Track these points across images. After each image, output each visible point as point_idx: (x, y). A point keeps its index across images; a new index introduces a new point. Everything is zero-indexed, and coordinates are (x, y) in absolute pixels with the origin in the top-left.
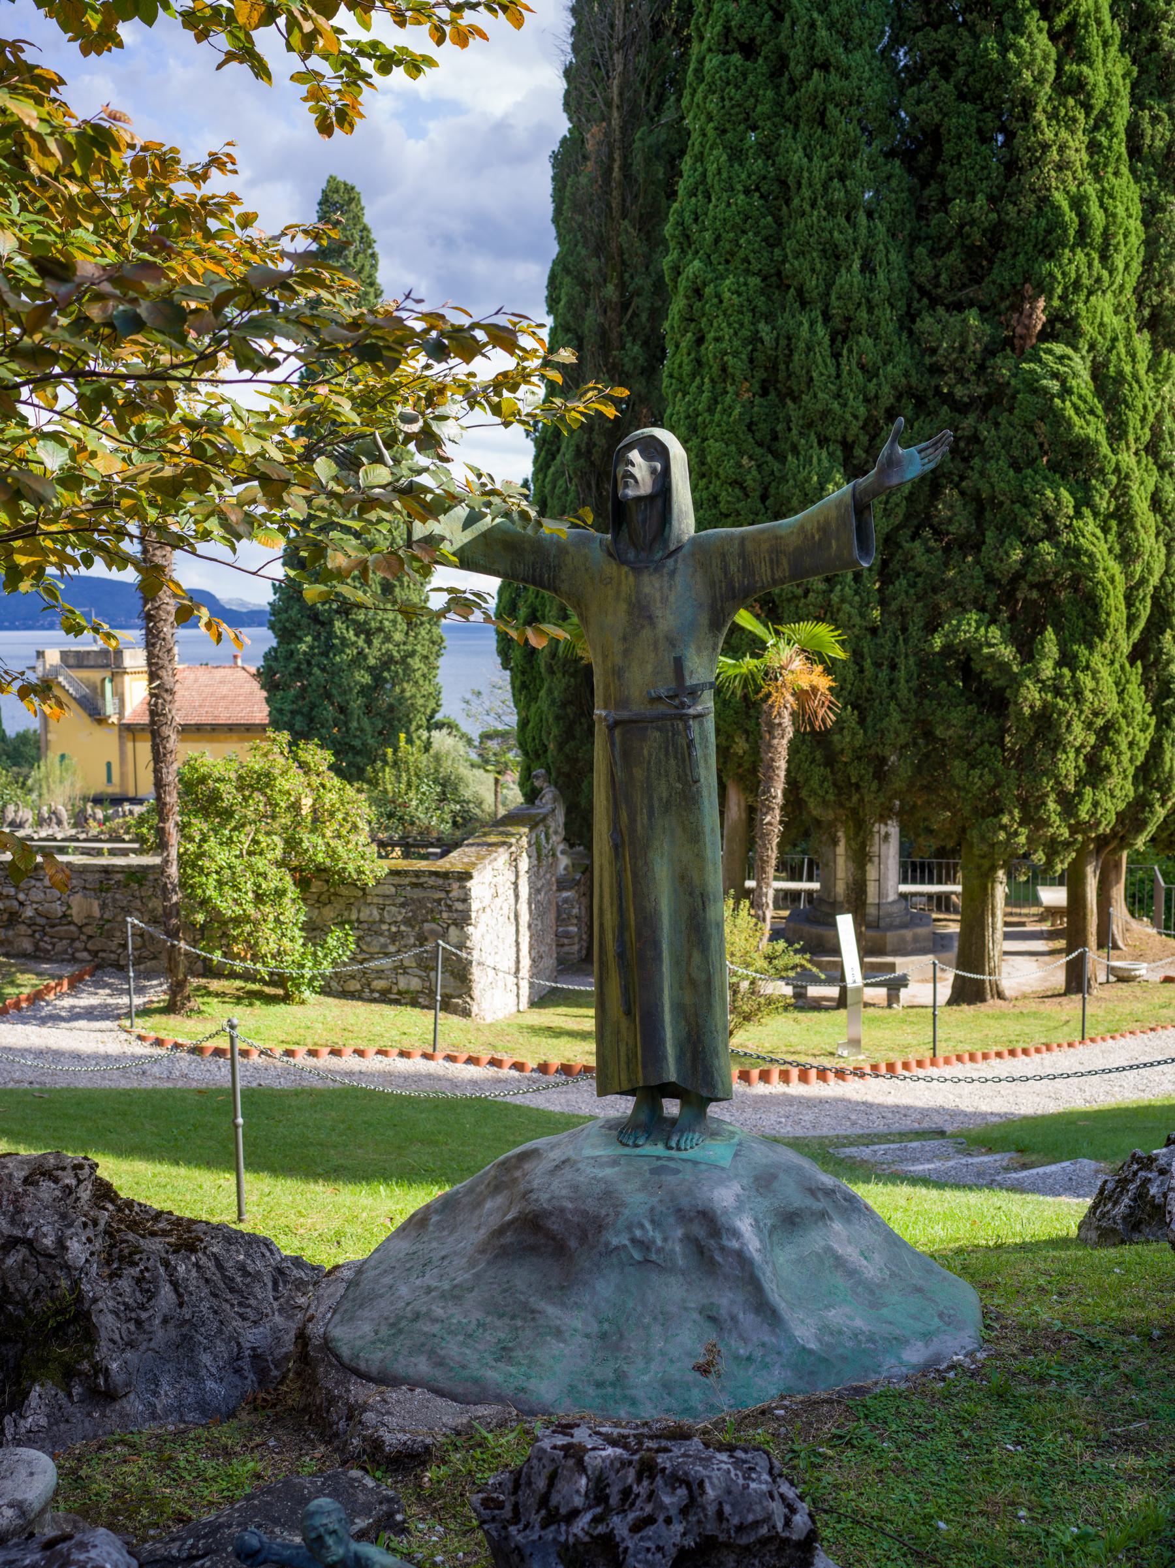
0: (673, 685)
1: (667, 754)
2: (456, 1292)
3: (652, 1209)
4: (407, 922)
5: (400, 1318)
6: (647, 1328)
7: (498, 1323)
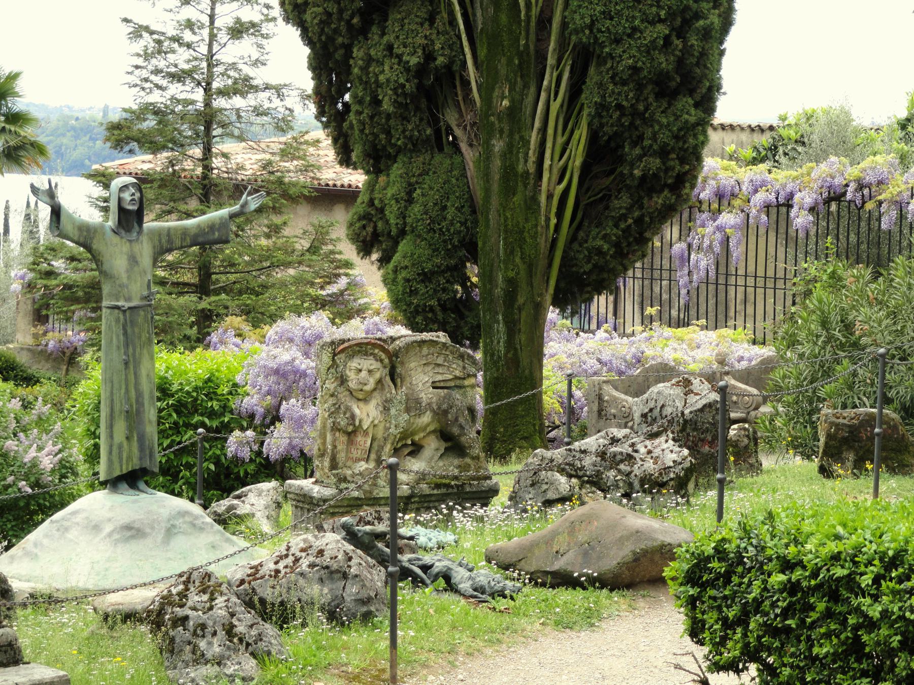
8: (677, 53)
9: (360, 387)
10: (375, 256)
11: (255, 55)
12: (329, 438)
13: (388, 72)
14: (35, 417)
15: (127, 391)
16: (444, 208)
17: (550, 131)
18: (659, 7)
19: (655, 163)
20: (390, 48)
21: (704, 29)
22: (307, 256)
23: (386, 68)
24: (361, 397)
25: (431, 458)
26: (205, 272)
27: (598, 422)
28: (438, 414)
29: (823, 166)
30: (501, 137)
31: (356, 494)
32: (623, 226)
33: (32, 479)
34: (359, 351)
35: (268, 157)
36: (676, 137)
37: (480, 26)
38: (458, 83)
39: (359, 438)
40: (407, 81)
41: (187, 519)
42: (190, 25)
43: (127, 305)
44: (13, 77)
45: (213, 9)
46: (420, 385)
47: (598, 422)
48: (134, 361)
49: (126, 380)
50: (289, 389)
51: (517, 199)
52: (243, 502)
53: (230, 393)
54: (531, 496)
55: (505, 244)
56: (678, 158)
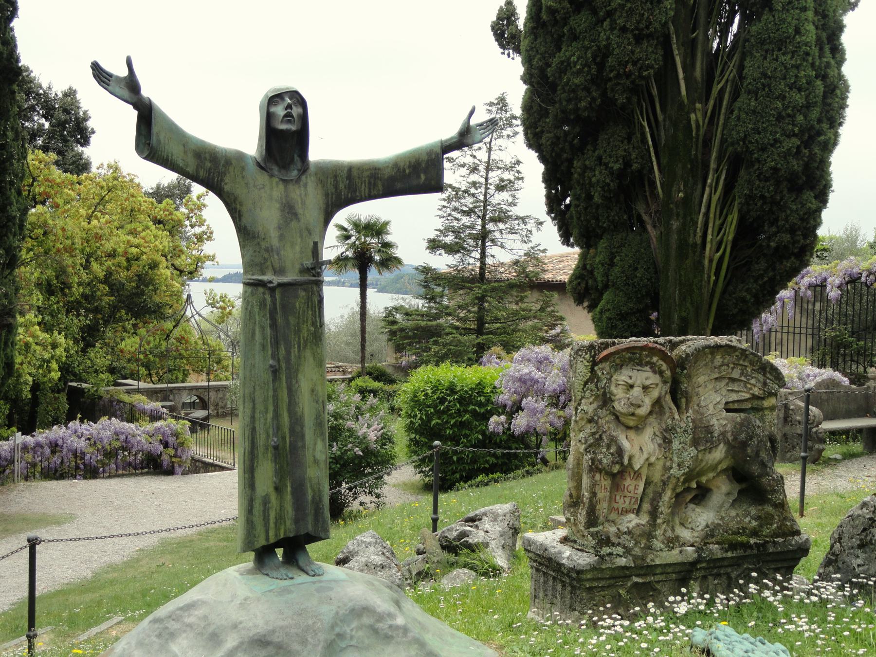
8: (806, 159)
9: (631, 410)
10: (586, 304)
11: (510, 200)
12: (586, 481)
13: (598, 175)
14: (368, 406)
15: (277, 415)
16: (636, 269)
17: (712, 215)
18: (794, 125)
19: (786, 237)
20: (600, 158)
21: (824, 142)
22: (539, 313)
23: (597, 173)
24: (631, 424)
25: (721, 506)
26: (481, 322)
27: (784, 426)
28: (734, 447)
29: (845, 262)
30: (677, 219)
31: (622, 561)
32: (760, 282)
33: (363, 446)
34: (631, 360)
35: (517, 257)
36: (802, 220)
37: (663, 142)
38: (646, 183)
39: (628, 482)
40: (612, 181)
41: (366, 620)
42: (474, 184)
43: (276, 280)
44: (386, 224)
45: (487, 175)
46: (711, 407)
47: (784, 426)
48: (288, 368)
49: (276, 397)
50: (528, 390)
51: (689, 262)
52: (477, 527)
53: (492, 392)
54: (859, 561)
55: (680, 293)
56: (802, 235)
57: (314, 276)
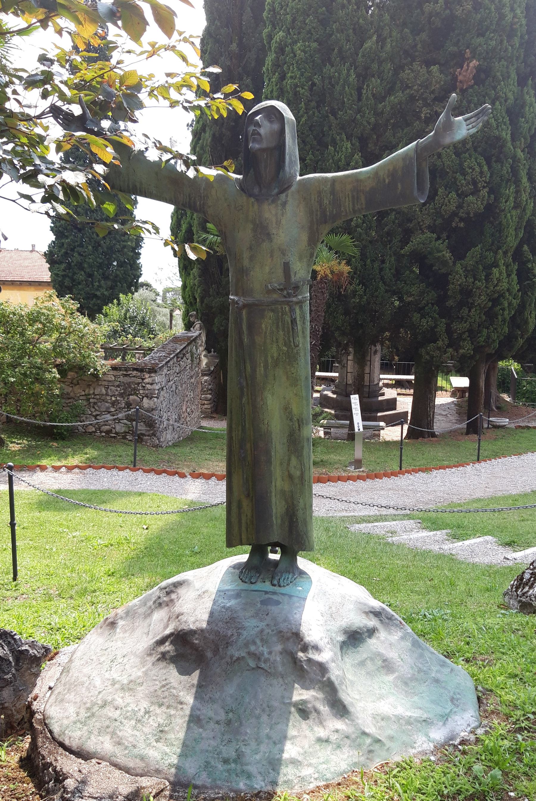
0: (283, 280)
1: (278, 327)
2: (131, 686)
3: (262, 631)
4: (121, 395)
5: (94, 704)
6: (258, 717)
7: (158, 711)
57: (285, 297)
